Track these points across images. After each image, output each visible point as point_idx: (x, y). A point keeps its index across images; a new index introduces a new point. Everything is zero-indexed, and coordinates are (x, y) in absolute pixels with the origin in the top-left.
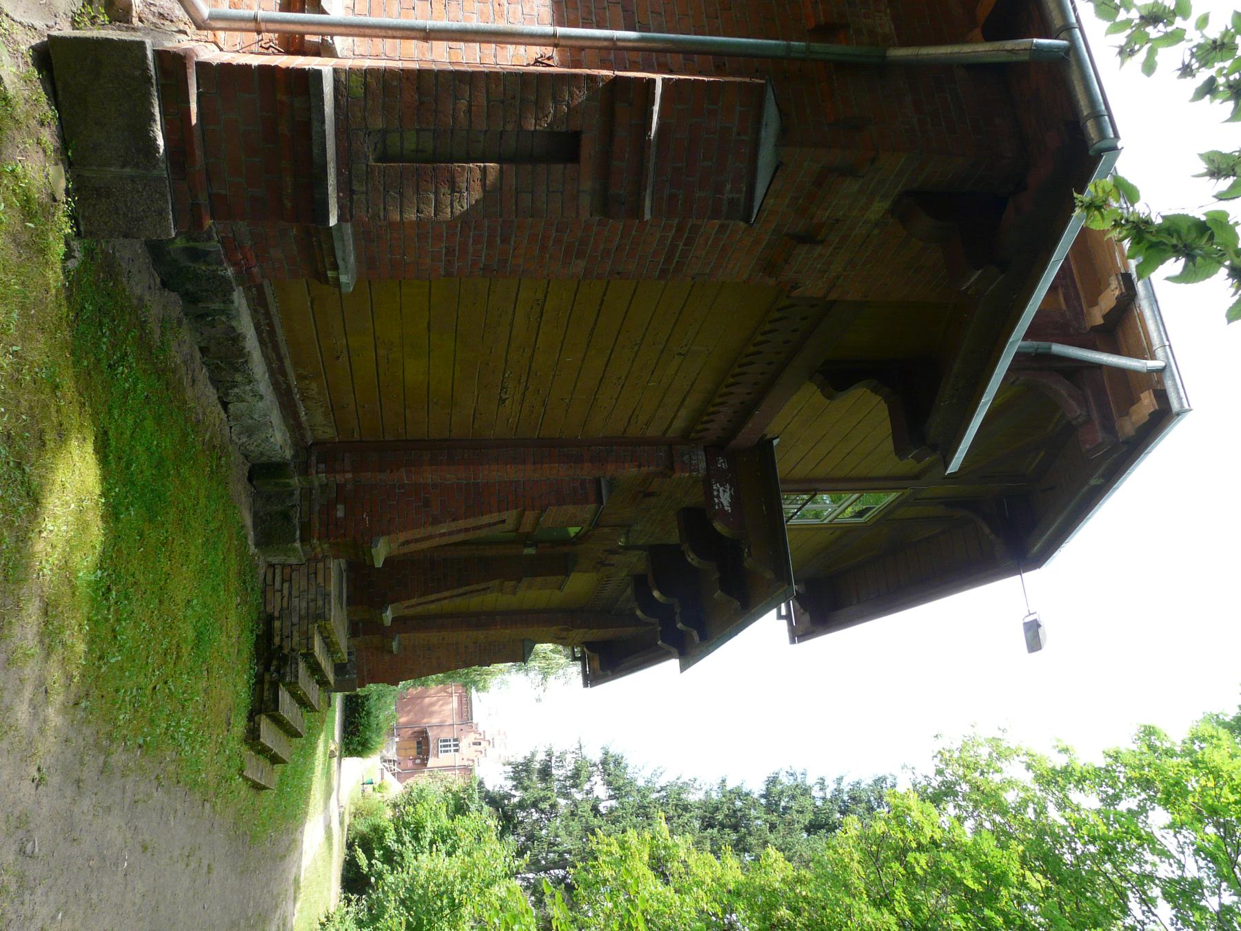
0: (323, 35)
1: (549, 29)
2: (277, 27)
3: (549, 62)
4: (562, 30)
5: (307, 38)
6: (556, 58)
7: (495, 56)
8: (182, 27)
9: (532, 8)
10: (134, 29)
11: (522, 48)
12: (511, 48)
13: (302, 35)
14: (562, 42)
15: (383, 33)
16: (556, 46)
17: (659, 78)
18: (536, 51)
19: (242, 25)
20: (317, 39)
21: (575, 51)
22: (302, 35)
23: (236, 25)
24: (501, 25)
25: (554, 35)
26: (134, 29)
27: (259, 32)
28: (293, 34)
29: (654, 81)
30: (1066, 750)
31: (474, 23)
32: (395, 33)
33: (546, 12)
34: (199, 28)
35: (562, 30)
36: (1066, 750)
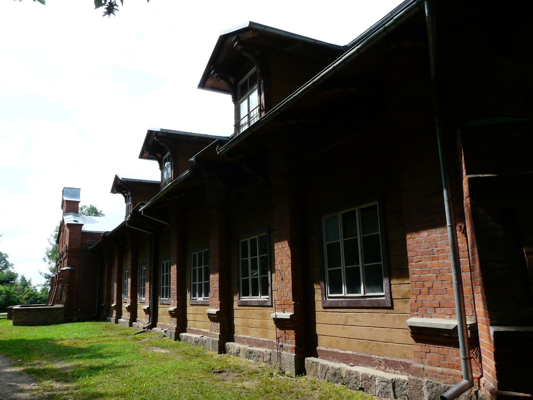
0: (467, 329)
1: (449, 229)
2: (467, 349)
3: (463, 227)
4: (448, 223)
5: (469, 336)
6: (460, 224)
7: (464, 251)
8: (473, 393)
9: (438, 237)
10: (469, 351)
11: (459, 240)
12: (459, 245)
13: (468, 339)
14: (454, 222)
15: (462, 302)
16: (456, 225)
17: (382, 263)
18: (460, 238)
19: (469, 365)
20: (469, 331)
21: (458, 216)
22: (468, 339)
23: (469, 369)
24: (449, 248)
25: (451, 226)
26: (469, 351)
27: (471, 358)
28: (469, 343)
29: (329, 271)
30: (44, 259)
31: (450, 261)
32: (462, 297)
33: (436, 234)
34: (473, 385)
35: (448, 223)
36: (44, 259)
